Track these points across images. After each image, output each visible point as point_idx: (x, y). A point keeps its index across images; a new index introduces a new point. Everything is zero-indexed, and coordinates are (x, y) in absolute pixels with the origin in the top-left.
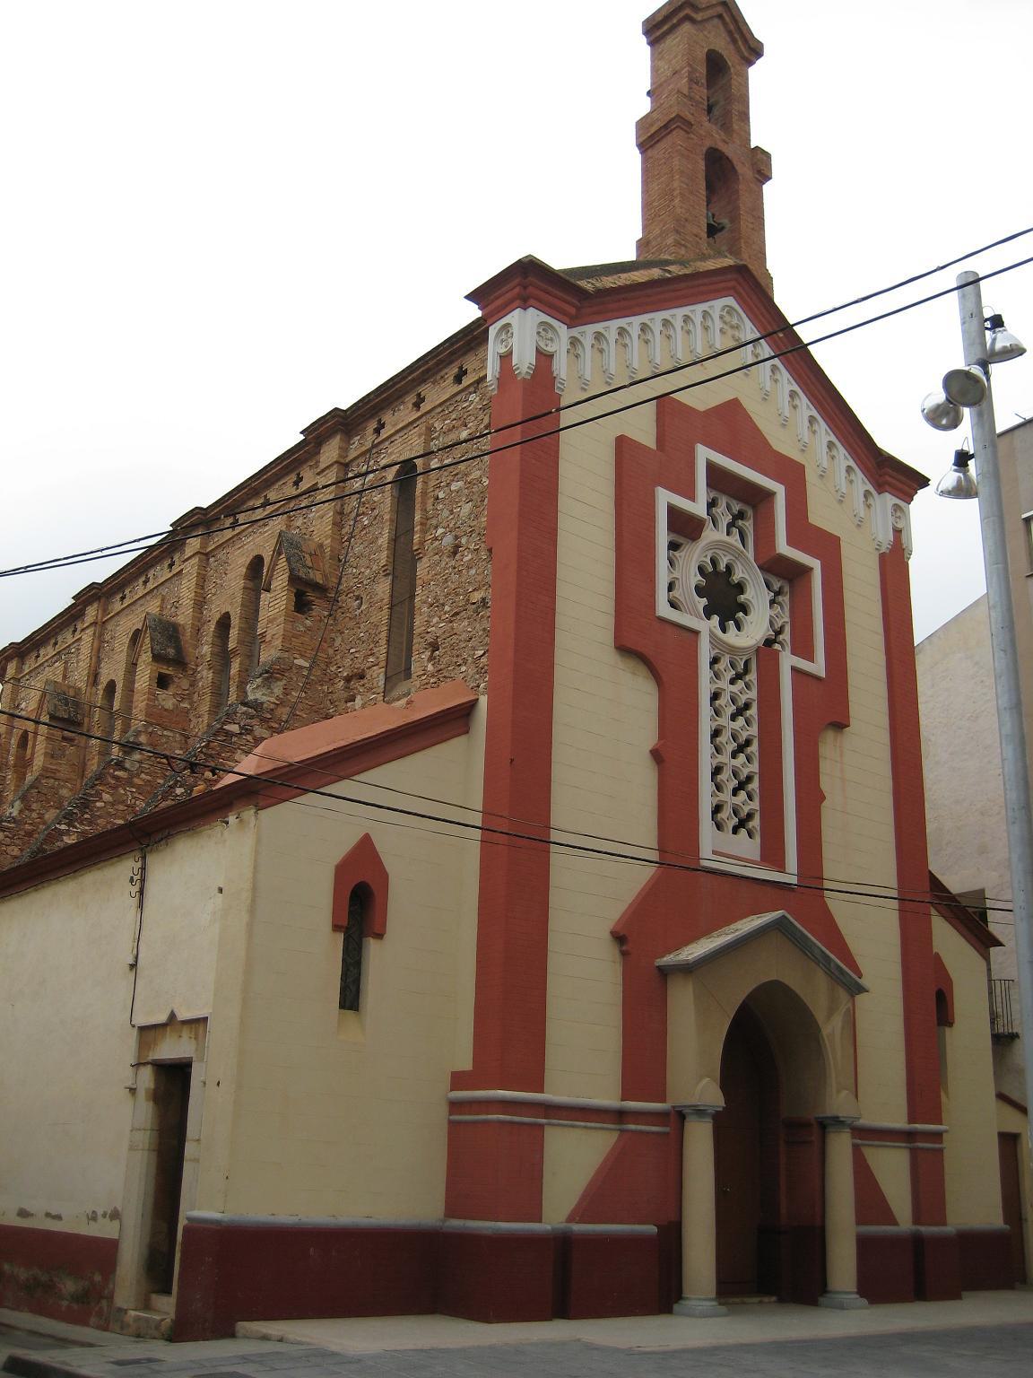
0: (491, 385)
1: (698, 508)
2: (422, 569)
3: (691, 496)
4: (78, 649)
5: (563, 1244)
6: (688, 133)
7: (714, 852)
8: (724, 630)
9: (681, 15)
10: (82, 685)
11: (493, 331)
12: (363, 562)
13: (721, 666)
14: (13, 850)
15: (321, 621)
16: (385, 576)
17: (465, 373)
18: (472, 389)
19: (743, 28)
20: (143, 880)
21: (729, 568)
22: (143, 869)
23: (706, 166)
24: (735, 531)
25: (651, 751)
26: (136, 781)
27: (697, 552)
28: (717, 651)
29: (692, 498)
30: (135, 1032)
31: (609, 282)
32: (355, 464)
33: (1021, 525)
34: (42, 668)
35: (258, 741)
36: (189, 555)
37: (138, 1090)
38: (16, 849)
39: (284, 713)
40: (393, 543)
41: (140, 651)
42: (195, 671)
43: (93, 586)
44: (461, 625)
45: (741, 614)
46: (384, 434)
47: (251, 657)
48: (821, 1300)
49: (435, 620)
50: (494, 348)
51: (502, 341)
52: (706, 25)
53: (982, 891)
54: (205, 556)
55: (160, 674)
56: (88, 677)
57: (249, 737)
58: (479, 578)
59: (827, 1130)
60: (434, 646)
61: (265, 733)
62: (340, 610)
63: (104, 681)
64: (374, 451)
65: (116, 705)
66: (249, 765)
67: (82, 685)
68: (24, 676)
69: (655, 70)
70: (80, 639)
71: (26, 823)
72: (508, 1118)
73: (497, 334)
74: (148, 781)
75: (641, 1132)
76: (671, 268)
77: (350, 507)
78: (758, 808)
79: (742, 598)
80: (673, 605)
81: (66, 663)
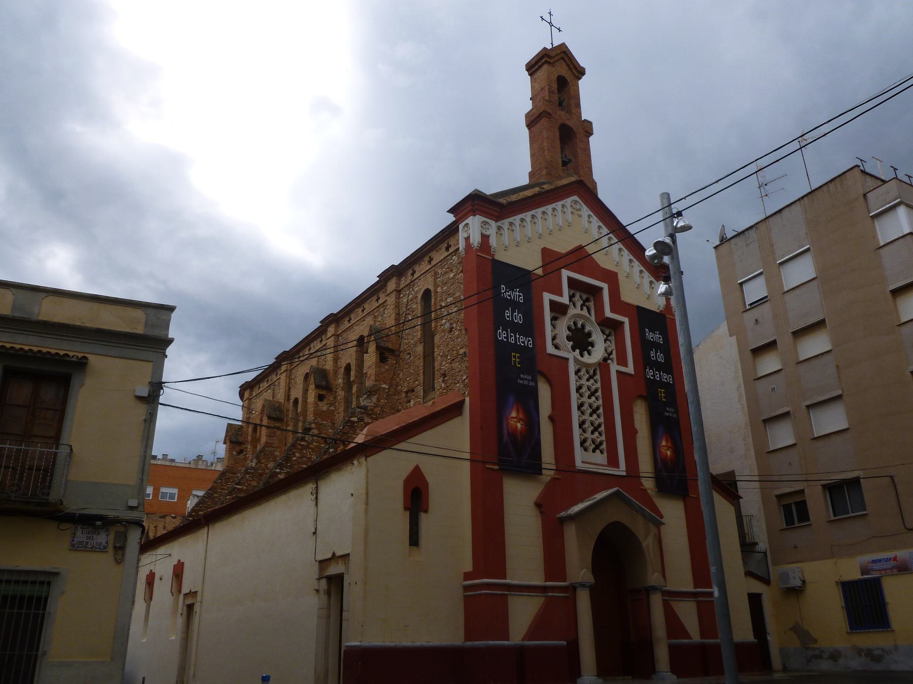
1: (565, 300)
2: (437, 339)
3: (560, 294)
4: (279, 383)
5: (520, 651)
7: (583, 462)
8: (582, 356)
9: (543, 61)
11: (461, 226)
12: (410, 337)
13: (581, 373)
14: (253, 483)
15: (392, 366)
16: (420, 343)
17: (450, 246)
18: (454, 254)
20: (317, 493)
21: (583, 326)
22: (317, 487)
23: (560, 133)
24: (585, 308)
25: (549, 417)
26: (311, 446)
27: (566, 321)
28: (579, 366)
29: (561, 295)
31: (514, 198)
33: (738, 286)
35: (367, 424)
39: (378, 410)
42: (336, 392)
43: (284, 352)
44: (456, 365)
45: (590, 348)
46: (416, 276)
47: (362, 383)
49: (444, 363)
50: (462, 235)
51: (465, 231)
53: (733, 472)
57: (362, 423)
58: (462, 343)
60: (444, 375)
61: (370, 421)
63: (292, 398)
64: (412, 284)
65: (299, 410)
66: (360, 439)
67: (282, 401)
69: (532, 87)
70: (280, 378)
73: (463, 227)
75: (492, 594)
76: (544, 186)
78: (605, 439)
79: (590, 340)
80: (557, 347)
81: (274, 390)
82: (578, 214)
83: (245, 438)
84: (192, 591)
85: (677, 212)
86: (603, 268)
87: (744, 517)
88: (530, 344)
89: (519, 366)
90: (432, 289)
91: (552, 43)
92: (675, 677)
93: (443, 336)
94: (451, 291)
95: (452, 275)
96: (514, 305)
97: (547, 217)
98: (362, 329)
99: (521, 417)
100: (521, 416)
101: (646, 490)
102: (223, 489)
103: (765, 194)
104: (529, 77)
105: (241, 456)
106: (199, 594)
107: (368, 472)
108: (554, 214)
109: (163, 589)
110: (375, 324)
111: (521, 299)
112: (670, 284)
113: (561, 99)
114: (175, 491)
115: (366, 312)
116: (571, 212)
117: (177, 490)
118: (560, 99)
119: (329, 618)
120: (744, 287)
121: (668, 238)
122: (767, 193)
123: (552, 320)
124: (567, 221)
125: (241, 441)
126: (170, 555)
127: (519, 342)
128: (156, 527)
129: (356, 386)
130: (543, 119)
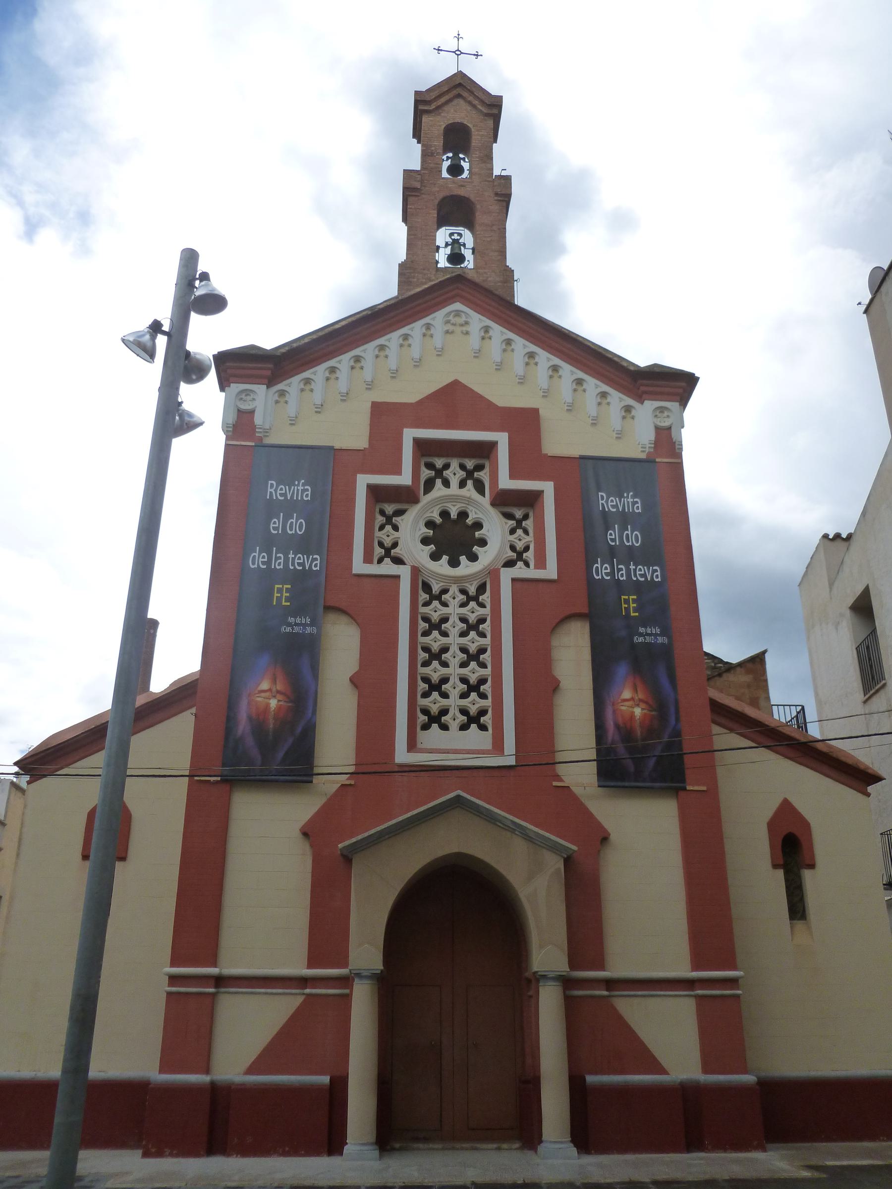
21: (463, 515)
24: (470, 483)
75: (179, 993)
89: (637, 614)
96: (625, 519)
100: (641, 696)
101: (569, 787)
111: (638, 508)
127: (635, 576)
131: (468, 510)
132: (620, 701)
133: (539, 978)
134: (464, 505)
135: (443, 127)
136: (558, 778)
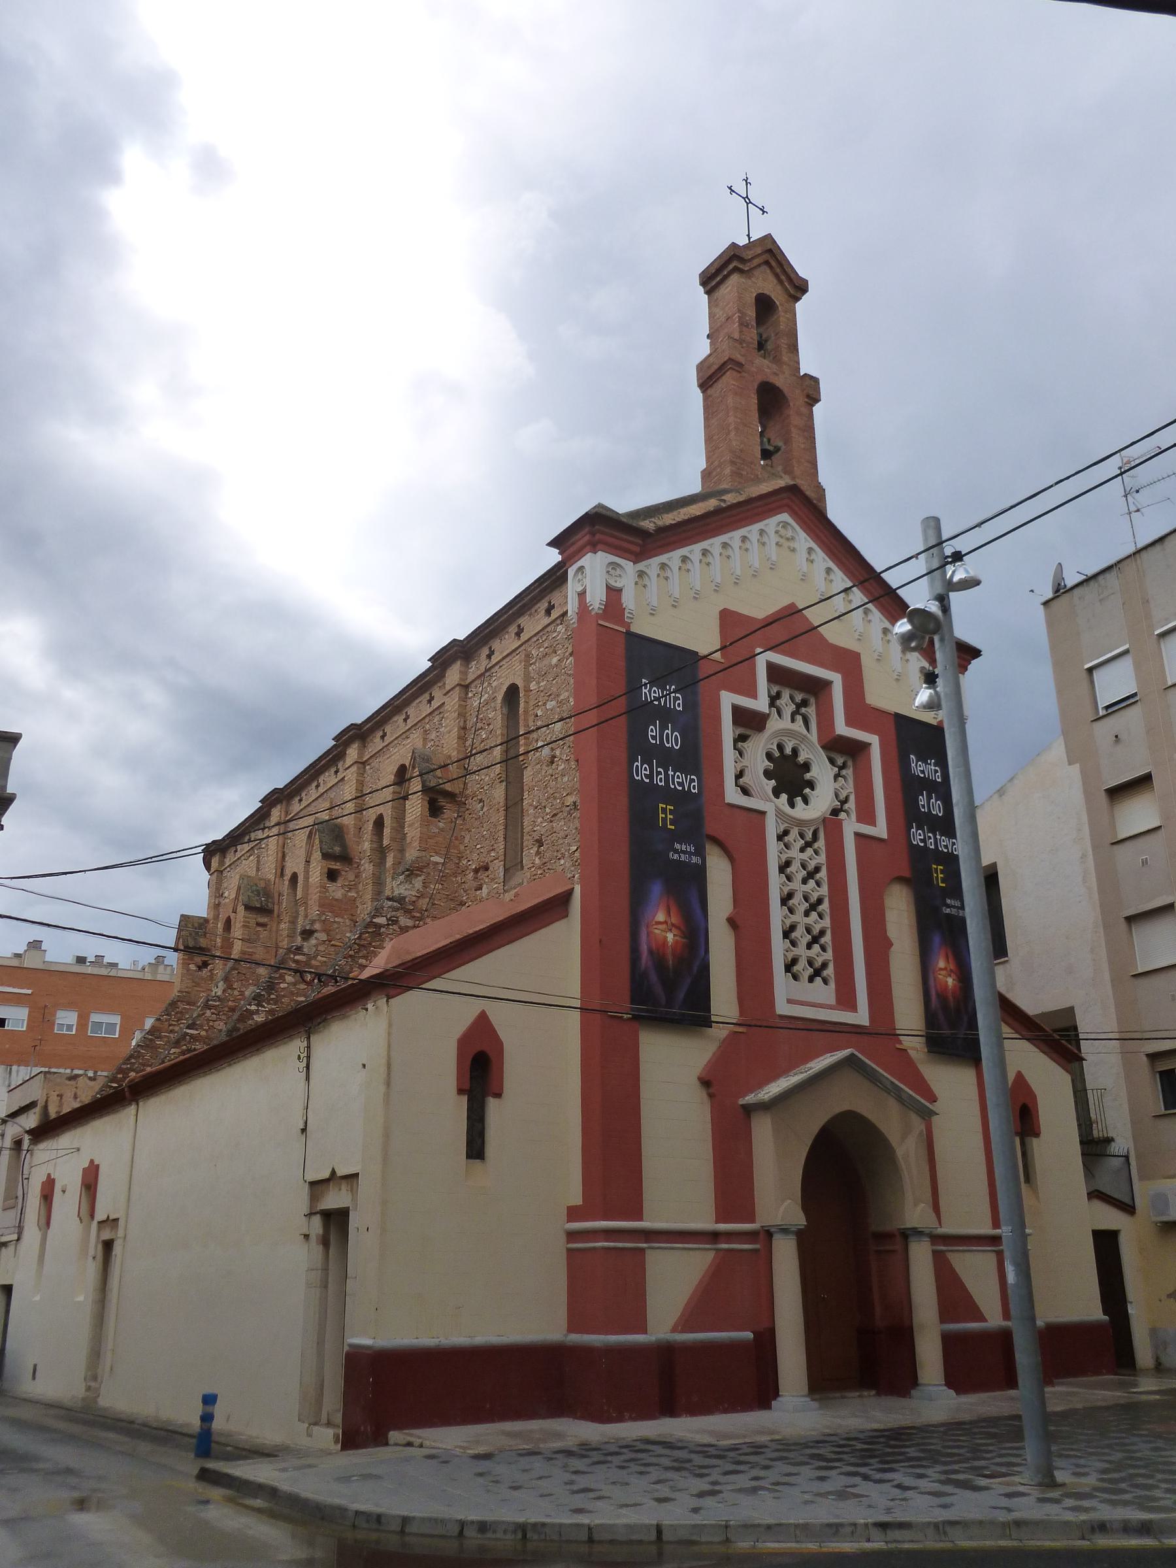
0: (571, 620)
1: (761, 704)
2: (528, 775)
5: (666, 1352)
6: (740, 372)
7: (789, 1001)
8: (792, 805)
9: (731, 267)
10: (271, 877)
11: (571, 572)
14: (219, 1025)
16: (500, 782)
18: (559, 622)
19: (789, 270)
20: (308, 1057)
21: (795, 751)
22: (309, 1047)
24: (799, 718)
26: (313, 962)
28: (787, 825)
29: (754, 695)
30: (307, 1185)
31: (669, 519)
32: (473, 685)
33: (1085, 675)
34: (240, 861)
36: (349, 765)
37: (310, 1236)
38: (222, 1024)
40: (505, 754)
41: (312, 850)
42: (359, 865)
43: (275, 791)
44: (559, 825)
45: (807, 790)
46: (494, 659)
48: (913, 1392)
49: (540, 820)
50: (572, 587)
51: (579, 581)
52: (755, 273)
54: (362, 764)
55: (329, 869)
56: (276, 870)
57: (395, 927)
58: (571, 785)
59: (909, 1240)
61: (410, 923)
62: (468, 812)
64: (487, 674)
65: (299, 894)
67: (271, 877)
68: (225, 869)
69: (711, 316)
71: (229, 1000)
72: (612, 1244)
73: (575, 575)
74: (325, 962)
77: (471, 723)
79: (808, 776)
80: (745, 791)
81: (258, 857)
82: (789, 548)
83: (211, 940)
84: (111, 1218)
85: (953, 553)
86: (832, 644)
87: (1089, 1093)
88: (694, 786)
90: (520, 684)
91: (748, 235)
92: (952, 1393)
93: (539, 772)
94: (554, 689)
95: (555, 660)
96: (665, 716)
97: (669, 574)
98: (400, 755)
99: (673, 922)
100: (674, 920)
101: (906, 1050)
102: (171, 1031)
103: (1136, 509)
104: (706, 296)
105: (205, 972)
106: (121, 1223)
107: (390, 1025)
108: (744, 547)
109: (67, 1205)
110: (424, 745)
111: (679, 704)
112: (938, 689)
113: (764, 336)
114: (116, 1019)
115: (410, 723)
116: (777, 544)
117: (119, 1017)
118: (760, 335)
119: (326, 1287)
120: (1095, 674)
121: (933, 602)
122: (1140, 507)
123: (736, 741)
124: (768, 560)
125: (204, 946)
126: (78, 1150)
127: (673, 784)
128: (60, 1096)
129: (392, 855)
130: (728, 373)
131: (800, 748)
132: (654, 923)
133: (906, 1235)
134: (798, 742)
135: (755, 295)
136: (900, 1042)
